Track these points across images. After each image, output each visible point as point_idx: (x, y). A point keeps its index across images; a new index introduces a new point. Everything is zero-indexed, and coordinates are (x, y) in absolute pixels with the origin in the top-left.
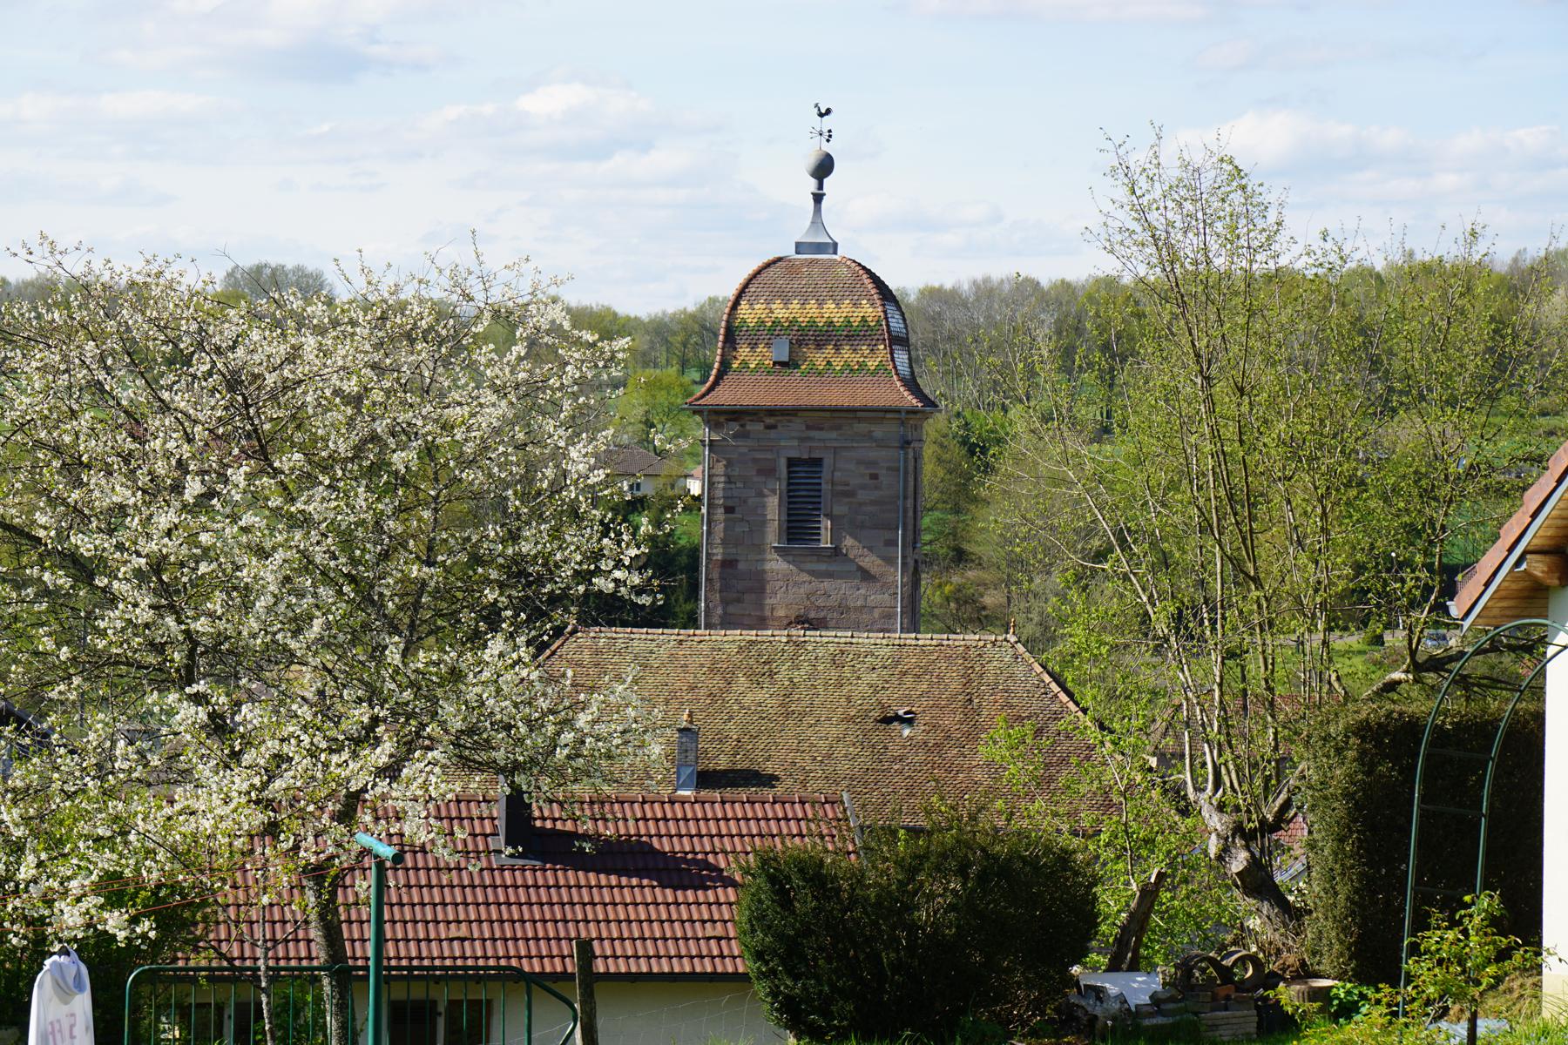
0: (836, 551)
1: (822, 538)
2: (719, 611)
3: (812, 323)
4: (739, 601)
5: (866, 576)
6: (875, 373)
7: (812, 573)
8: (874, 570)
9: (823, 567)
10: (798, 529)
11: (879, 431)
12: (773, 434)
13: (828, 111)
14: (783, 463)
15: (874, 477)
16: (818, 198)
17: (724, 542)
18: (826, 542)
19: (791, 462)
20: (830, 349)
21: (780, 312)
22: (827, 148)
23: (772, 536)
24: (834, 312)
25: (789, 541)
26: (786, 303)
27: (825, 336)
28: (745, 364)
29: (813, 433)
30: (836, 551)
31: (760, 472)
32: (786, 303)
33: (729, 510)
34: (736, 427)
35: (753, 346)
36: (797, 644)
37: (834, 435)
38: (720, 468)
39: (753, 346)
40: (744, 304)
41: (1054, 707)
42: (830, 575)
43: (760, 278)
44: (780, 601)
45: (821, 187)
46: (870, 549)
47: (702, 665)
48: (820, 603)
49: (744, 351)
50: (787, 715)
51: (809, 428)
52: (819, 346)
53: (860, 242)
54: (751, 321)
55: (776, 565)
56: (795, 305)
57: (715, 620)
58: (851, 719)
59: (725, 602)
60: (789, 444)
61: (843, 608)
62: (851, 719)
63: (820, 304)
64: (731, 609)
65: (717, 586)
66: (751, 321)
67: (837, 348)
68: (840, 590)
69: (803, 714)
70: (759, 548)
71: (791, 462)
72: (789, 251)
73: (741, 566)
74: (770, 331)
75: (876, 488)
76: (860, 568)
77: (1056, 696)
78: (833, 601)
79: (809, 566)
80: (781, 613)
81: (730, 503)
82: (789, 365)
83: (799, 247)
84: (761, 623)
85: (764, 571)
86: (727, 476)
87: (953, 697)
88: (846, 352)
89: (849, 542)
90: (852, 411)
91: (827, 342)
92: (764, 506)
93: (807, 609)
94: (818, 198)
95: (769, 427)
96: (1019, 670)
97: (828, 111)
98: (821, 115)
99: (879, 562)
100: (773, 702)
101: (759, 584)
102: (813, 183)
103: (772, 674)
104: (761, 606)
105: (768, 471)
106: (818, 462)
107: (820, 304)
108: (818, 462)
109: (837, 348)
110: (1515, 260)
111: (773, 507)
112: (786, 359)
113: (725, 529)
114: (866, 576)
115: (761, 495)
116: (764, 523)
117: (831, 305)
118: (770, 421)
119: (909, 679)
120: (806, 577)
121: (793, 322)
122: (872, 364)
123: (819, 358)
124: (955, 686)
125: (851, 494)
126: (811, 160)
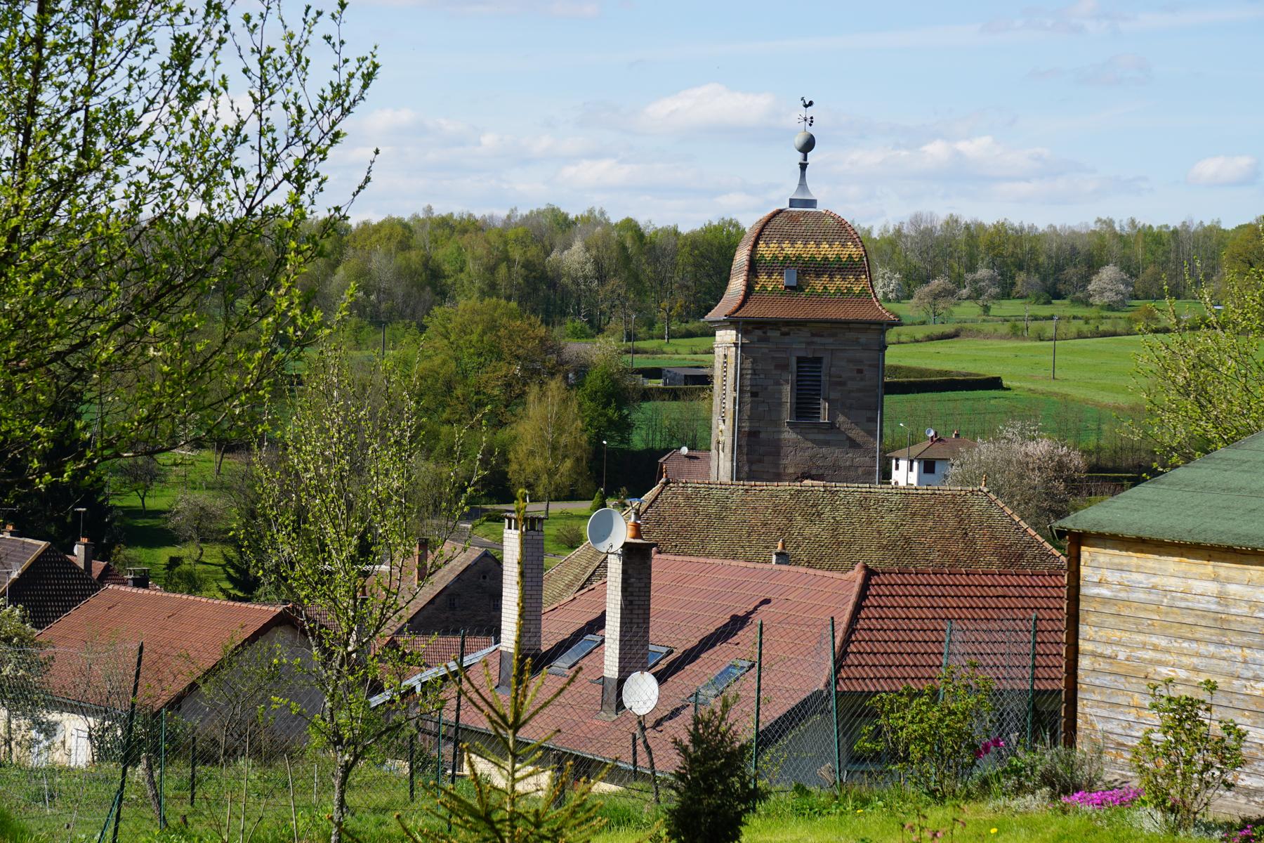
0: (832, 426)
1: (822, 416)
2: (746, 469)
3: (813, 258)
4: (760, 461)
5: (854, 444)
6: (859, 295)
7: (813, 441)
8: (859, 440)
9: (821, 437)
10: (804, 409)
11: (863, 338)
12: (787, 339)
13: (811, 103)
14: (794, 360)
15: (860, 371)
16: (803, 167)
17: (751, 418)
18: (824, 418)
19: (800, 360)
20: (825, 278)
21: (789, 250)
22: (811, 130)
23: (786, 415)
24: (828, 250)
25: (798, 417)
26: (793, 243)
27: (823, 268)
28: (764, 287)
29: (816, 339)
30: (832, 426)
31: (777, 367)
32: (793, 243)
33: (754, 394)
34: (759, 333)
35: (770, 275)
36: (832, 493)
37: (831, 340)
38: (748, 364)
39: (770, 275)
40: (761, 244)
41: (1027, 539)
42: (827, 443)
43: (771, 225)
44: (790, 463)
45: (805, 159)
46: (857, 424)
47: (767, 508)
48: (819, 463)
49: (763, 278)
50: (839, 544)
51: (813, 335)
52: (818, 275)
53: (831, 198)
54: (768, 257)
55: (789, 435)
56: (799, 244)
57: (743, 475)
58: (885, 547)
59: (750, 462)
60: (799, 346)
61: (836, 467)
62: (885, 547)
63: (818, 245)
64: (754, 467)
65: (745, 450)
66: (768, 257)
67: (831, 277)
68: (835, 454)
69: (850, 544)
70: (777, 423)
71: (800, 360)
72: (785, 205)
73: (762, 436)
74: (783, 264)
75: (862, 380)
76: (849, 439)
77: (1025, 530)
78: (829, 462)
79: (811, 436)
80: (791, 470)
81: (755, 390)
82: (796, 289)
83: (793, 203)
84: (778, 477)
85: (779, 440)
86: (754, 370)
87: (953, 533)
88: (838, 281)
89: (841, 418)
90: (846, 325)
91: (824, 272)
92: (780, 392)
93: (810, 468)
94: (803, 167)
95: (784, 334)
96: (994, 511)
97: (811, 103)
98: (806, 106)
99: (862, 433)
100: (825, 535)
101: (775, 449)
102: (800, 156)
103: (819, 515)
104: (777, 465)
105: (784, 367)
106: (819, 360)
107: (818, 245)
108: (819, 360)
109: (831, 277)
110: (509, 217)
111: (787, 393)
112: (794, 284)
113: (752, 408)
114: (854, 444)
115: (778, 383)
116: (780, 404)
117: (825, 245)
118: (784, 329)
119: (918, 518)
120: (810, 444)
121: (799, 257)
122: (857, 289)
123: (818, 284)
124: (952, 523)
125: (843, 384)
126: (799, 140)
